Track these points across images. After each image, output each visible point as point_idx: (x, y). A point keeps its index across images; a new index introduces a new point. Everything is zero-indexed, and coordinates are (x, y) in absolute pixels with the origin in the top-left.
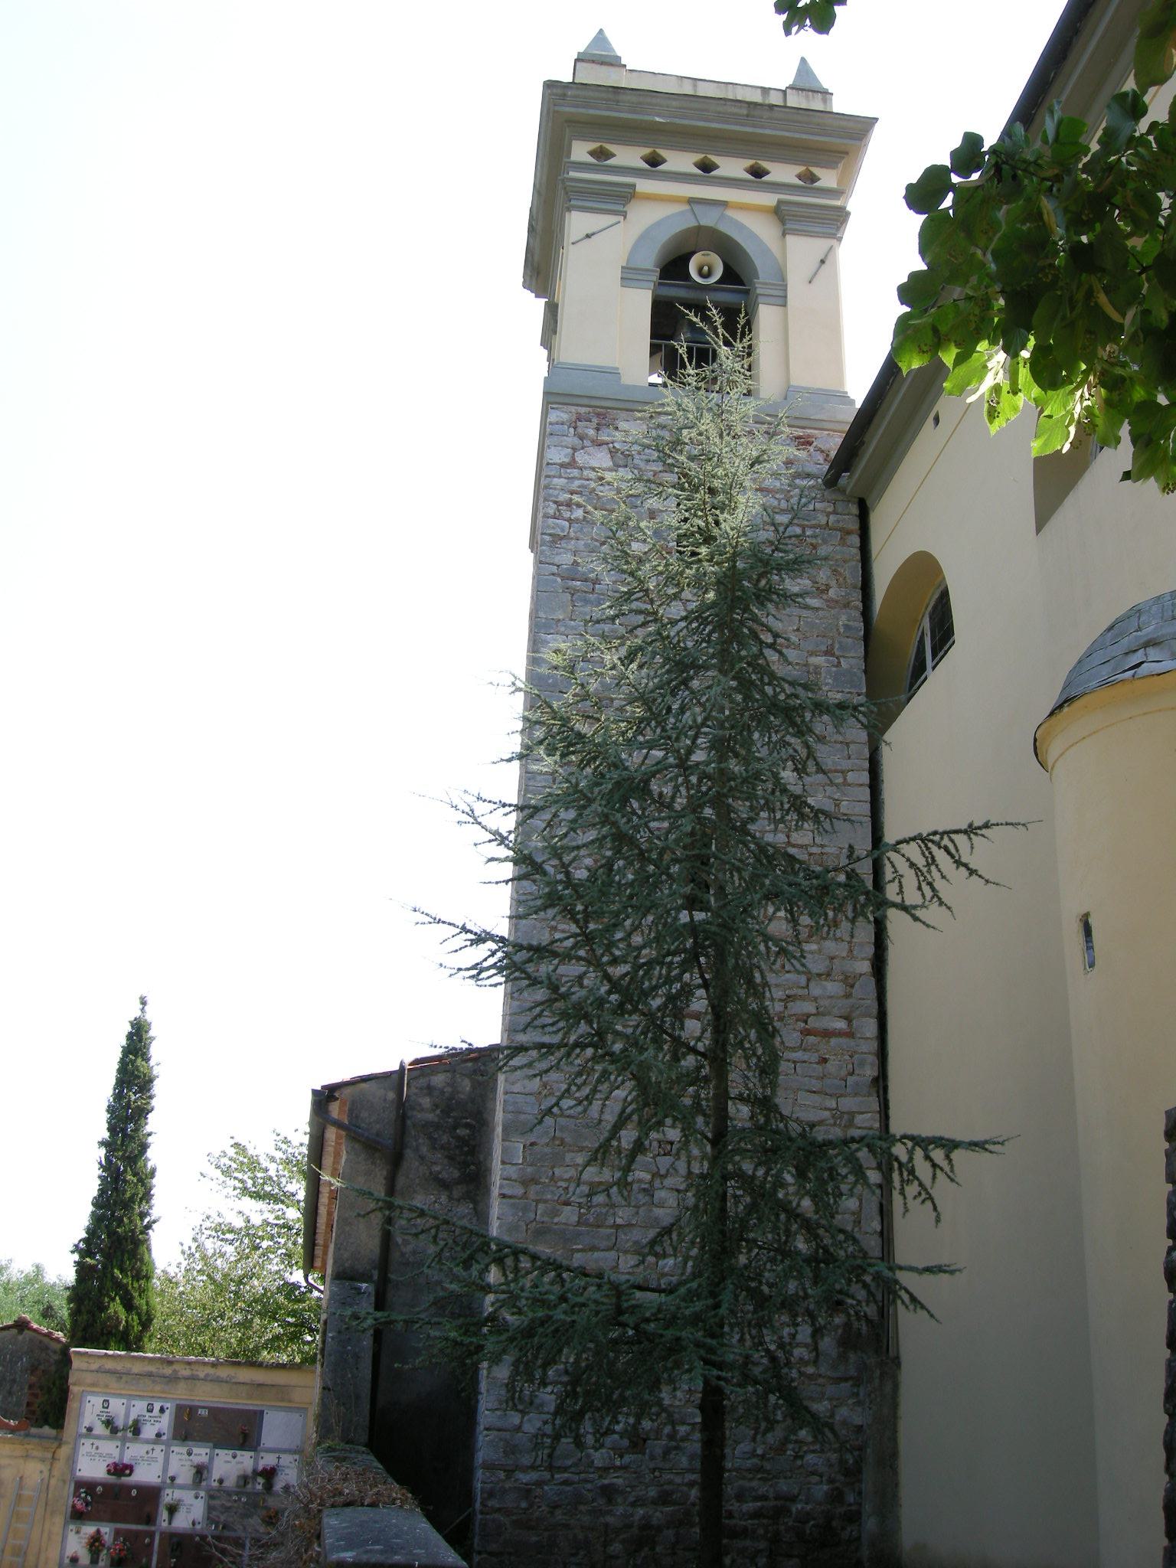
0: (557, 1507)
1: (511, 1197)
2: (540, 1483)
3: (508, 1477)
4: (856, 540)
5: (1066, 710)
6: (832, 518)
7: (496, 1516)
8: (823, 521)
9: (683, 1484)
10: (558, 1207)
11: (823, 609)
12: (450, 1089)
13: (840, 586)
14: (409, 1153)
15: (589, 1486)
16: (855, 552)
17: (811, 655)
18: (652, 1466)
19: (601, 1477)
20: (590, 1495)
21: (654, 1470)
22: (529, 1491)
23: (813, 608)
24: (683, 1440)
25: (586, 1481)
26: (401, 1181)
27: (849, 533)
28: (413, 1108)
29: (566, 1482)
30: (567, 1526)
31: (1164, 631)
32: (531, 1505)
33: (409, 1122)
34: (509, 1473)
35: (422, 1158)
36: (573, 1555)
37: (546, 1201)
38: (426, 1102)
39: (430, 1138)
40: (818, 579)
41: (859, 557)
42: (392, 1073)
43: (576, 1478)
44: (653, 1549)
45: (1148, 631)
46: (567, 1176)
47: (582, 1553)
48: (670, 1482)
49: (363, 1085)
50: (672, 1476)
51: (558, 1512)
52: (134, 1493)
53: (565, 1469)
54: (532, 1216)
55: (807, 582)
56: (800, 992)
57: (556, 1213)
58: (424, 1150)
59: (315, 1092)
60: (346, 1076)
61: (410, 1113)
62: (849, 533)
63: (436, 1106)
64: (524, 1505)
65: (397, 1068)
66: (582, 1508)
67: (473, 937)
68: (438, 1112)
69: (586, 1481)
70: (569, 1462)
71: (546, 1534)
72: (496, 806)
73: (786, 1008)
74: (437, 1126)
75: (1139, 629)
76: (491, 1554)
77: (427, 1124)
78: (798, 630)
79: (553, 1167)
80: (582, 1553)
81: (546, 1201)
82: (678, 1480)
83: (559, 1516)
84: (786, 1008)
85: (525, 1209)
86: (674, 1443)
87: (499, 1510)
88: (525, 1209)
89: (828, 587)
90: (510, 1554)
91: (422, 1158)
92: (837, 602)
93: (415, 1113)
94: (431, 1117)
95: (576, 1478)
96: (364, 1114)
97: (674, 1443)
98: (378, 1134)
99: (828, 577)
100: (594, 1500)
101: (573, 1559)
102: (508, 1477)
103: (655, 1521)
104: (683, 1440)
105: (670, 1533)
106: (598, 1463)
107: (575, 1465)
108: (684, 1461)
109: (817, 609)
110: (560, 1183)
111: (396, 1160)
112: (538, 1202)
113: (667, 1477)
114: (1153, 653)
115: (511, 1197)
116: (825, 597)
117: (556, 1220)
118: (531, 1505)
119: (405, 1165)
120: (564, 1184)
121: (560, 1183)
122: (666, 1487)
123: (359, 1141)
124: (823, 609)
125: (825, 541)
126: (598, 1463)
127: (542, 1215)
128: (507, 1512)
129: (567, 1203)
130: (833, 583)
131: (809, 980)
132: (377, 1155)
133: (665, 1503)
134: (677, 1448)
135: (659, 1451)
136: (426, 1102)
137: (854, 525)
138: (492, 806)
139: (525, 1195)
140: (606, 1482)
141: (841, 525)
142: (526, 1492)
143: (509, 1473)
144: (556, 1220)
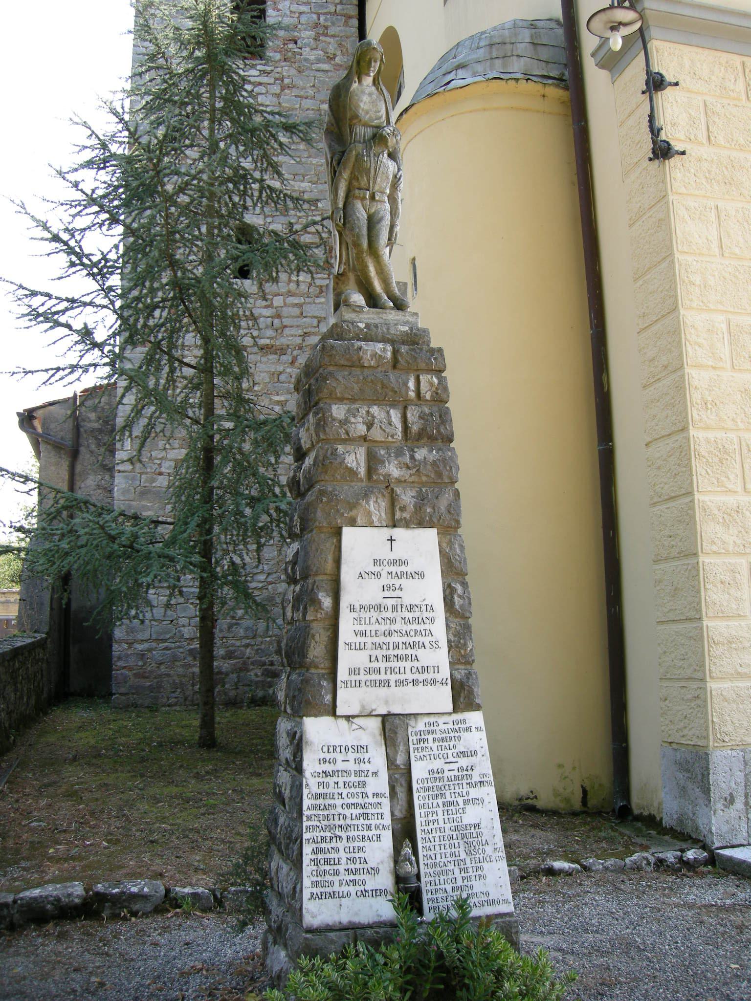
0: (160, 664)
1: (123, 472)
2: (150, 650)
3: (130, 647)
4: (355, 22)
5: (404, 116)
6: (339, 7)
7: (123, 671)
8: (333, 10)
9: (242, 646)
10: (155, 476)
11: (331, 71)
12: (108, 407)
13: (343, 55)
14: (83, 449)
15: (181, 650)
16: (355, 31)
17: (322, 103)
18: (221, 635)
19: (188, 644)
20: (182, 655)
21: (223, 638)
22: (143, 655)
23: (323, 71)
24: (240, 619)
25: (179, 647)
26: (78, 468)
27: (350, 17)
28: (84, 420)
29: (166, 649)
30: (168, 675)
31: (470, 58)
32: (145, 664)
33: (82, 430)
34: (130, 644)
35: (92, 452)
36: (173, 692)
37: (147, 473)
38: (93, 416)
39: (96, 438)
40: (328, 50)
41: (357, 34)
42: (69, 399)
43: (173, 645)
44: (223, 686)
45: (460, 59)
46: (160, 456)
47: (179, 690)
48: (233, 645)
49: (51, 407)
50: (233, 642)
51: (162, 667)
52: (624, 745)
53: (166, 640)
54: (138, 483)
55: (321, 52)
56: (313, 330)
57: (153, 480)
58: (93, 447)
59: (19, 414)
60: (39, 403)
61: (82, 424)
62: (350, 17)
63: (100, 418)
64: (140, 663)
65: (72, 395)
66: (178, 663)
67: (27, 292)
68: (101, 422)
69: (179, 647)
70: (168, 636)
71: (155, 681)
72: (56, 205)
73: (304, 340)
74: (100, 431)
75: (455, 57)
76: (121, 694)
77: (93, 430)
78: (314, 86)
79: (150, 451)
80: (179, 690)
81: (147, 473)
82: (238, 643)
83: (163, 669)
84: (304, 340)
85: (133, 479)
86: (234, 621)
87: (125, 667)
88: (133, 479)
89: (335, 55)
90: (133, 694)
91: (92, 452)
92: (341, 66)
93: (86, 423)
94: (96, 425)
95: (173, 645)
96: (52, 426)
97: (234, 621)
98: (62, 438)
99: (335, 49)
100: (184, 659)
101: (173, 695)
102: (130, 647)
103: (224, 670)
104: (240, 619)
105: (234, 676)
106: (186, 636)
107: (172, 637)
108: (242, 632)
109: (327, 71)
110: (156, 461)
111: (74, 454)
112: (141, 474)
113: (230, 642)
114: (461, 73)
115: (123, 472)
116: (333, 62)
117: (154, 485)
118: (145, 664)
119: (81, 457)
120: (158, 462)
121: (156, 461)
122: (231, 648)
123: (49, 444)
124: (331, 71)
125: (333, 24)
126: (186, 636)
127: (145, 483)
128: (130, 669)
129: (160, 474)
130: (339, 53)
131: (319, 322)
132: (62, 452)
133: (230, 658)
134: (237, 624)
135: (225, 626)
136: (93, 416)
137: (354, 11)
138: (54, 205)
139: (133, 471)
140: (192, 647)
141: (345, 12)
142: (142, 656)
143: (130, 644)
144: (154, 485)
